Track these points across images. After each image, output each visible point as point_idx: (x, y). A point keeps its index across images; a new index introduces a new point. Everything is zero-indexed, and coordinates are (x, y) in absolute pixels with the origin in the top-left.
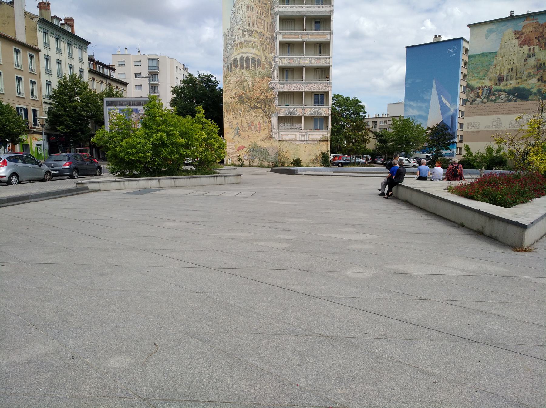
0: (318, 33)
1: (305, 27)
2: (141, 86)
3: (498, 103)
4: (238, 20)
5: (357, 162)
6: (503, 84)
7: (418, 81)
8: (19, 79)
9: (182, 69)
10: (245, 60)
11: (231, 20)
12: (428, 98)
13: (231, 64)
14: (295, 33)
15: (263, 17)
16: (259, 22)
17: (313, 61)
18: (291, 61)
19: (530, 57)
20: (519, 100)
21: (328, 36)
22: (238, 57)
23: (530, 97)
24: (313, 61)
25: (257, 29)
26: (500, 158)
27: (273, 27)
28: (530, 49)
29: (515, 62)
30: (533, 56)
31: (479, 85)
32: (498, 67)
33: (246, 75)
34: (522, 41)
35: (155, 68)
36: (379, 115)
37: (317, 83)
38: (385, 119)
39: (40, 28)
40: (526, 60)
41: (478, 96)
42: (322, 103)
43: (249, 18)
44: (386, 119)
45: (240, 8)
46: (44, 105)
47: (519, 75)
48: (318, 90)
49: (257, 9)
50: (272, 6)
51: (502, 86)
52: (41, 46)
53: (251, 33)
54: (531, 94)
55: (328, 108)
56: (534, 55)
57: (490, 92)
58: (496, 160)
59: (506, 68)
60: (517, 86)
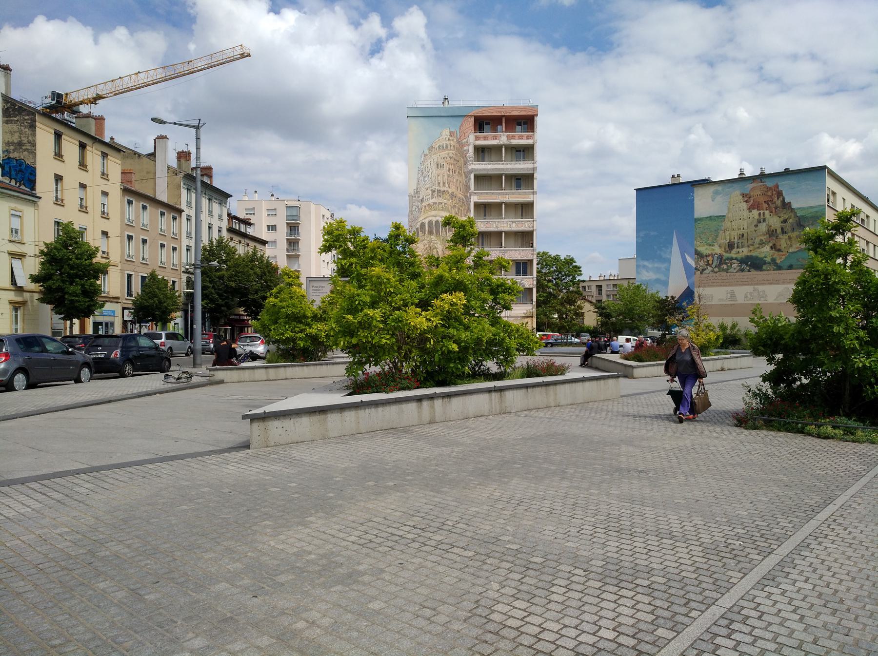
0: (519, 193)
1: (503, 186)
2: (275, 241)
3: (731, 272)
4: (426, 179)
5: (569, 342)
6: (734, 251)
7: (652, 233)
8: (162, 246)
9: (330, 219)
10: (434, 224)
11: (418, 179)
12: (668, 257)
13: (417, 229)
14: (493, 193)
15: (456, 175)
16: (450, 181)
17: (514, 225)
18: (488, 225)
19: (760, 222)
20: (752, 270)
21: (531, 196)
22: (426, 221)
23: (764, 267)
24: (514, 225)
25: (448, 189)
26: (734, 336)
27: (467, 187)
28: (760, 214)
29: (745, 227)
30: (763, 221)
31: (708, 252)
32: (728, 233)
33: (435, 242)
34: (751, 205)
35: (295, 218)
36: (605, 276)
37: (519, 250)
38: (616, 283)
39: (184, 184)
40: (756, 226)
41: (708, 265)
42: (525, 273)
43: (439, 177)
44: (615, 283)
45: (429, 166)
46: (182, 274)
47: (750, 242)
48: (519, 258)
49: (448, 167)
50: (465, 163)
51: (733, 254)
52: (183, 206)
53: (441, 193)
54: (765, 263)
55: (533, 278)
56: (764, 220)
57: (721, 260)
58: (730, 339)
59: (736, 233)
60: (749, 254)
